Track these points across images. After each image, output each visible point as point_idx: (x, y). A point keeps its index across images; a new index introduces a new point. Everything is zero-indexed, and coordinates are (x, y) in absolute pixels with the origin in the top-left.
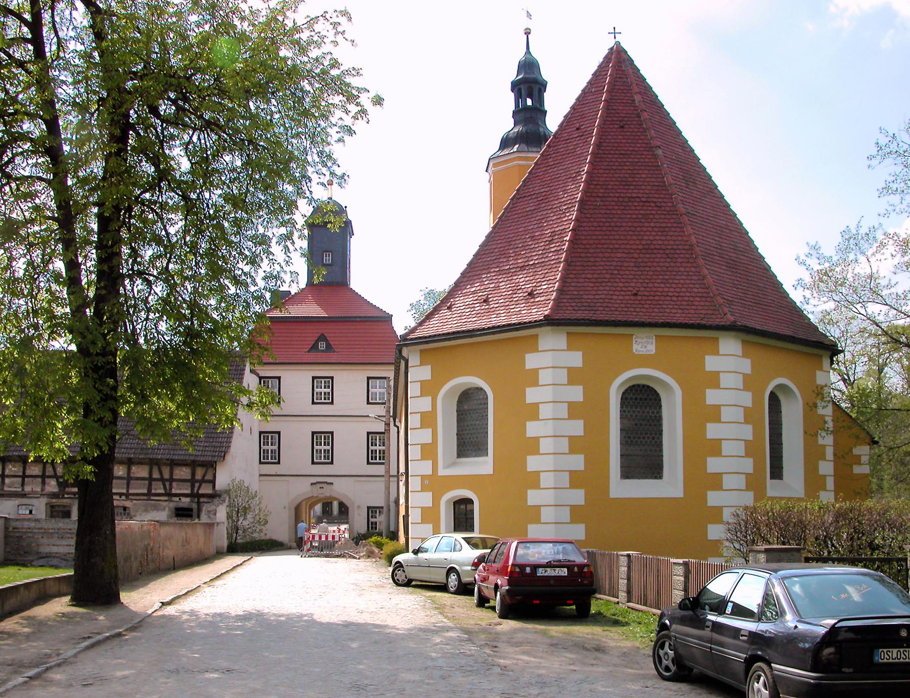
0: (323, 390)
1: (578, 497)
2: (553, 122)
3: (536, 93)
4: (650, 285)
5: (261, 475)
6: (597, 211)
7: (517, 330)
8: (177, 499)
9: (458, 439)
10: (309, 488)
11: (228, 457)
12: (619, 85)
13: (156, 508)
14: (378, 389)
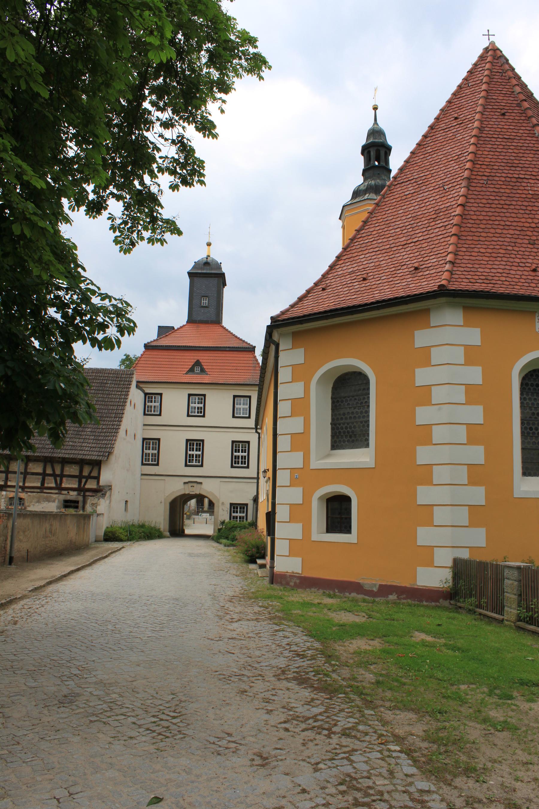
0: (197, 405)
1: (478, 495)
5: (142, 475)
6: (484, 189)
8: (66, 492)
9: (333, 429)
11: (113, 458)
13: (48, 500)
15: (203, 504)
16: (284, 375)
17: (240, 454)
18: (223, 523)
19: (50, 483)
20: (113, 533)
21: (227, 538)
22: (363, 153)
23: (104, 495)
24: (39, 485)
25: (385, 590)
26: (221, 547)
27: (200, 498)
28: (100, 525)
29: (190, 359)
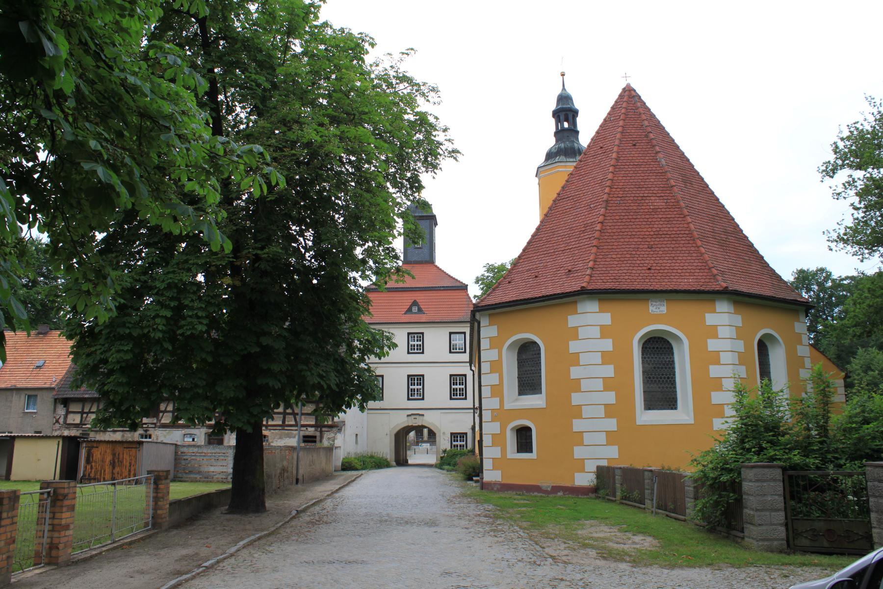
1: (612, 424)
2: (585, 139)
3: (570, 117)
4: (661, 261)
7: (561, 298)
10: (405, 419)
12: (630, 108)
13: (289, 436)
14: (458, 341)
15: (422, 434)
16: (485, 344)
17: (458, 387)
18: (445, 451)
19: (290, 421)
20: (350, 463)
21: (449, 464)
22: (554, 116)
23: (340, 430)
24: (280, 423)
25: (556, 489)
26: (445, 472)
27: (419, 429)
28: (339, 456)
29: (407, 299)
